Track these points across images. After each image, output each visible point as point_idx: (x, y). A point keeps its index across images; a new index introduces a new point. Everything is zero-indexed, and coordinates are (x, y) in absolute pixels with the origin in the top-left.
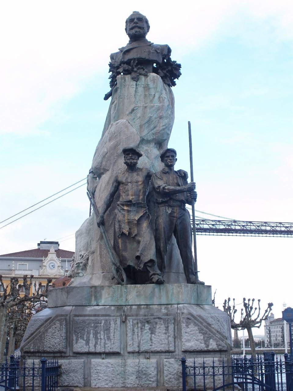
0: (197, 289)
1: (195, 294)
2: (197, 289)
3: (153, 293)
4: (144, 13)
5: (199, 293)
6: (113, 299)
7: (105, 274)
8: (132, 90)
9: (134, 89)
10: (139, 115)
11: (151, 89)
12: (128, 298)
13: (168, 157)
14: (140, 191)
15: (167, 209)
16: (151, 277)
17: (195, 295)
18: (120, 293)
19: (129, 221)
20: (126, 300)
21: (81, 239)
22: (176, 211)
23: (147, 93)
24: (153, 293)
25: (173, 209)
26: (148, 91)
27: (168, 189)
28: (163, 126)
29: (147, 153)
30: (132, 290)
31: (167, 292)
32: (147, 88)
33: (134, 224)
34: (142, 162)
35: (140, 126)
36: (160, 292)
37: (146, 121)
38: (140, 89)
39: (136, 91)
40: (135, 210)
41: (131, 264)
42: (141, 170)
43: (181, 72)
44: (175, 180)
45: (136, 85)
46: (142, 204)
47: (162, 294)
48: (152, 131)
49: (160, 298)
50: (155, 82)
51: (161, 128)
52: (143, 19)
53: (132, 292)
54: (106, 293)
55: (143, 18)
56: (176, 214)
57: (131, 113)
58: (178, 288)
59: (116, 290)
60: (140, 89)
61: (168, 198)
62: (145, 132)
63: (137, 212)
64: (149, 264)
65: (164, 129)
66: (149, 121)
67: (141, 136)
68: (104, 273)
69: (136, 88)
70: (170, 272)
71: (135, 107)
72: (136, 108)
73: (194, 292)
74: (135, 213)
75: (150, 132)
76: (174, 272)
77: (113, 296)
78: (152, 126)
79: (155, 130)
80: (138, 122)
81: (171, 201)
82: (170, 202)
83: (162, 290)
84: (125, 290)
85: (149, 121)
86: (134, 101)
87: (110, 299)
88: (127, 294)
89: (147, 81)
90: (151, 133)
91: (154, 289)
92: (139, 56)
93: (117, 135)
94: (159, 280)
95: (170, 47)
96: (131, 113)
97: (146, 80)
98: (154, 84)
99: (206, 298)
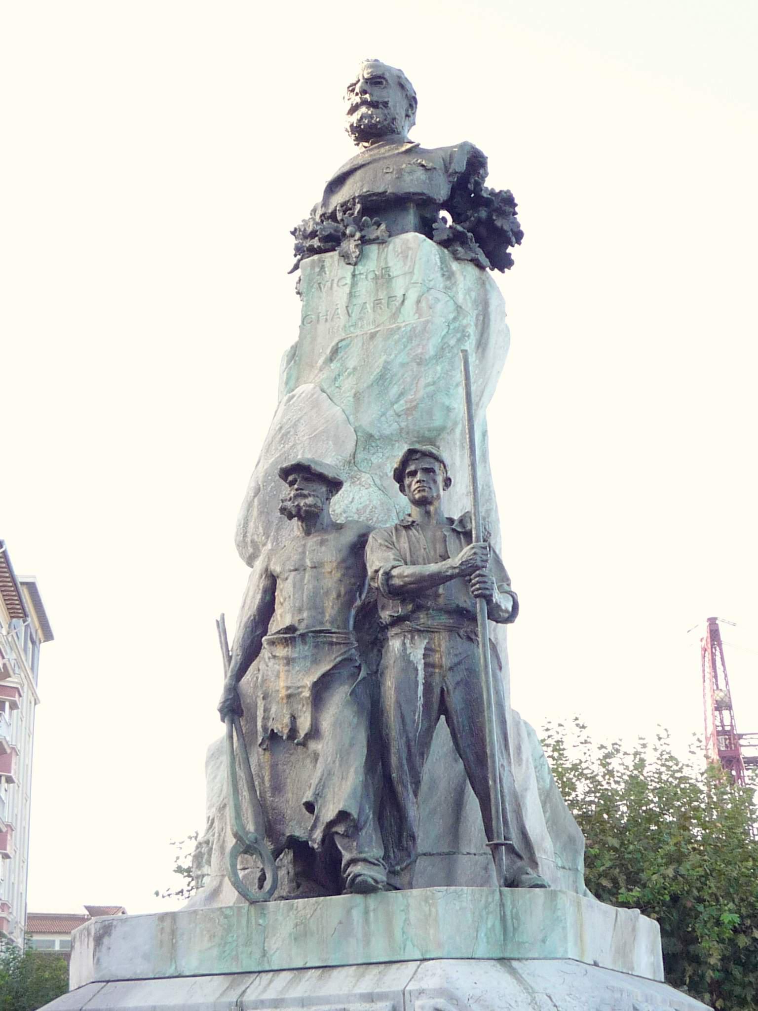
0: (502, 905)
1: (493, 921)
2: (502, 905)
3: (345, 923)
4: (392, 61)
5: (509, 917)
6: (224, 952)
7: (248, 873)
8: (341, 294)
9: (347, 289)
10: (351, 364)
11: (394, 281)
12: (270, 948)
13: (413, 474)
14: (327, 593)
15: (408, 642)
16: (345, 871)
17: (493, 926)
18: (245, 930)
19: (289, 692)
20: (264, 954)
21: (218, 768)
22: (440, 645)
23: (382, 295)
24: (345, 923)
25: (431, 639)
26: (387, 287)
27: (400, 576)
28: (428, 385)
29: (381, 477)
30: (280, 918)
31: (389, 923)
32: (384, 278)
33: (302, 699)
34: (343, 506)
35: (355, 395)
36: (367, 921)
37: (372, 377)
38: (365, 287)
39: (351, 295)
40: (305, 657)
41: (297, 834)
42: (339, 527)
43: (518, 220)
44: (438, 546)
45: (354, 276)
46: (334, 633)
47: (373, 926)
48: (396, 406)
49: (367, 942)
50: (407, 257)
51: (421, 393)
52: (384, 78)
53: (281, 924)
54: (205, 932)
55: (387, 76)
56: (437, 655)
57: (331, 360)
58: (423, 904)
59: (234, 920)
60: (365, 287)
61: (410, 607)
62: (368, 417)
63: (315, 661)
64: (340, 829)
65: (431, 396)
66: (383, 379)
67: (357, 424)
68: (246, 871)
69: (354, 285)
70: (454, 853)
71: (342, 340)
72: (344, 343)
73: (488, 913)
74: (308, 664)
75: (387, 410)
76: (473, 851)
77: (226, 943)
78: (394, 391)
79: (402, 402)
80: (348, 384)
81: (422, 616)
82: (419, 618)
83: (372, 914)
84: (261, 921)
85: (382, 377)
86: (345, 326)
87: (215, 952)
88: (265, 932)
89: (386, 258)
90: (391, 412)
91: (349, 912)
92: (365, 190)
93: (289, 432)
94: (359, 879)
95: (479, 146)
96: (331, 360)
97: (383, 256)
98: (405, 264)
99: (540, 937)
